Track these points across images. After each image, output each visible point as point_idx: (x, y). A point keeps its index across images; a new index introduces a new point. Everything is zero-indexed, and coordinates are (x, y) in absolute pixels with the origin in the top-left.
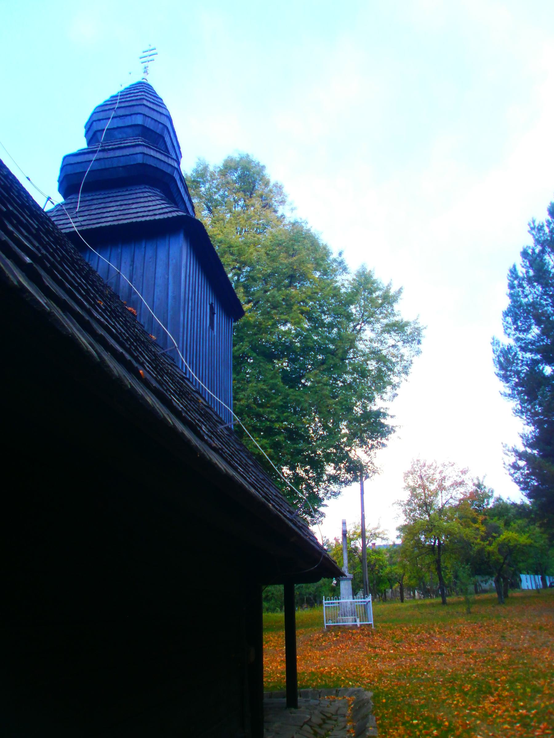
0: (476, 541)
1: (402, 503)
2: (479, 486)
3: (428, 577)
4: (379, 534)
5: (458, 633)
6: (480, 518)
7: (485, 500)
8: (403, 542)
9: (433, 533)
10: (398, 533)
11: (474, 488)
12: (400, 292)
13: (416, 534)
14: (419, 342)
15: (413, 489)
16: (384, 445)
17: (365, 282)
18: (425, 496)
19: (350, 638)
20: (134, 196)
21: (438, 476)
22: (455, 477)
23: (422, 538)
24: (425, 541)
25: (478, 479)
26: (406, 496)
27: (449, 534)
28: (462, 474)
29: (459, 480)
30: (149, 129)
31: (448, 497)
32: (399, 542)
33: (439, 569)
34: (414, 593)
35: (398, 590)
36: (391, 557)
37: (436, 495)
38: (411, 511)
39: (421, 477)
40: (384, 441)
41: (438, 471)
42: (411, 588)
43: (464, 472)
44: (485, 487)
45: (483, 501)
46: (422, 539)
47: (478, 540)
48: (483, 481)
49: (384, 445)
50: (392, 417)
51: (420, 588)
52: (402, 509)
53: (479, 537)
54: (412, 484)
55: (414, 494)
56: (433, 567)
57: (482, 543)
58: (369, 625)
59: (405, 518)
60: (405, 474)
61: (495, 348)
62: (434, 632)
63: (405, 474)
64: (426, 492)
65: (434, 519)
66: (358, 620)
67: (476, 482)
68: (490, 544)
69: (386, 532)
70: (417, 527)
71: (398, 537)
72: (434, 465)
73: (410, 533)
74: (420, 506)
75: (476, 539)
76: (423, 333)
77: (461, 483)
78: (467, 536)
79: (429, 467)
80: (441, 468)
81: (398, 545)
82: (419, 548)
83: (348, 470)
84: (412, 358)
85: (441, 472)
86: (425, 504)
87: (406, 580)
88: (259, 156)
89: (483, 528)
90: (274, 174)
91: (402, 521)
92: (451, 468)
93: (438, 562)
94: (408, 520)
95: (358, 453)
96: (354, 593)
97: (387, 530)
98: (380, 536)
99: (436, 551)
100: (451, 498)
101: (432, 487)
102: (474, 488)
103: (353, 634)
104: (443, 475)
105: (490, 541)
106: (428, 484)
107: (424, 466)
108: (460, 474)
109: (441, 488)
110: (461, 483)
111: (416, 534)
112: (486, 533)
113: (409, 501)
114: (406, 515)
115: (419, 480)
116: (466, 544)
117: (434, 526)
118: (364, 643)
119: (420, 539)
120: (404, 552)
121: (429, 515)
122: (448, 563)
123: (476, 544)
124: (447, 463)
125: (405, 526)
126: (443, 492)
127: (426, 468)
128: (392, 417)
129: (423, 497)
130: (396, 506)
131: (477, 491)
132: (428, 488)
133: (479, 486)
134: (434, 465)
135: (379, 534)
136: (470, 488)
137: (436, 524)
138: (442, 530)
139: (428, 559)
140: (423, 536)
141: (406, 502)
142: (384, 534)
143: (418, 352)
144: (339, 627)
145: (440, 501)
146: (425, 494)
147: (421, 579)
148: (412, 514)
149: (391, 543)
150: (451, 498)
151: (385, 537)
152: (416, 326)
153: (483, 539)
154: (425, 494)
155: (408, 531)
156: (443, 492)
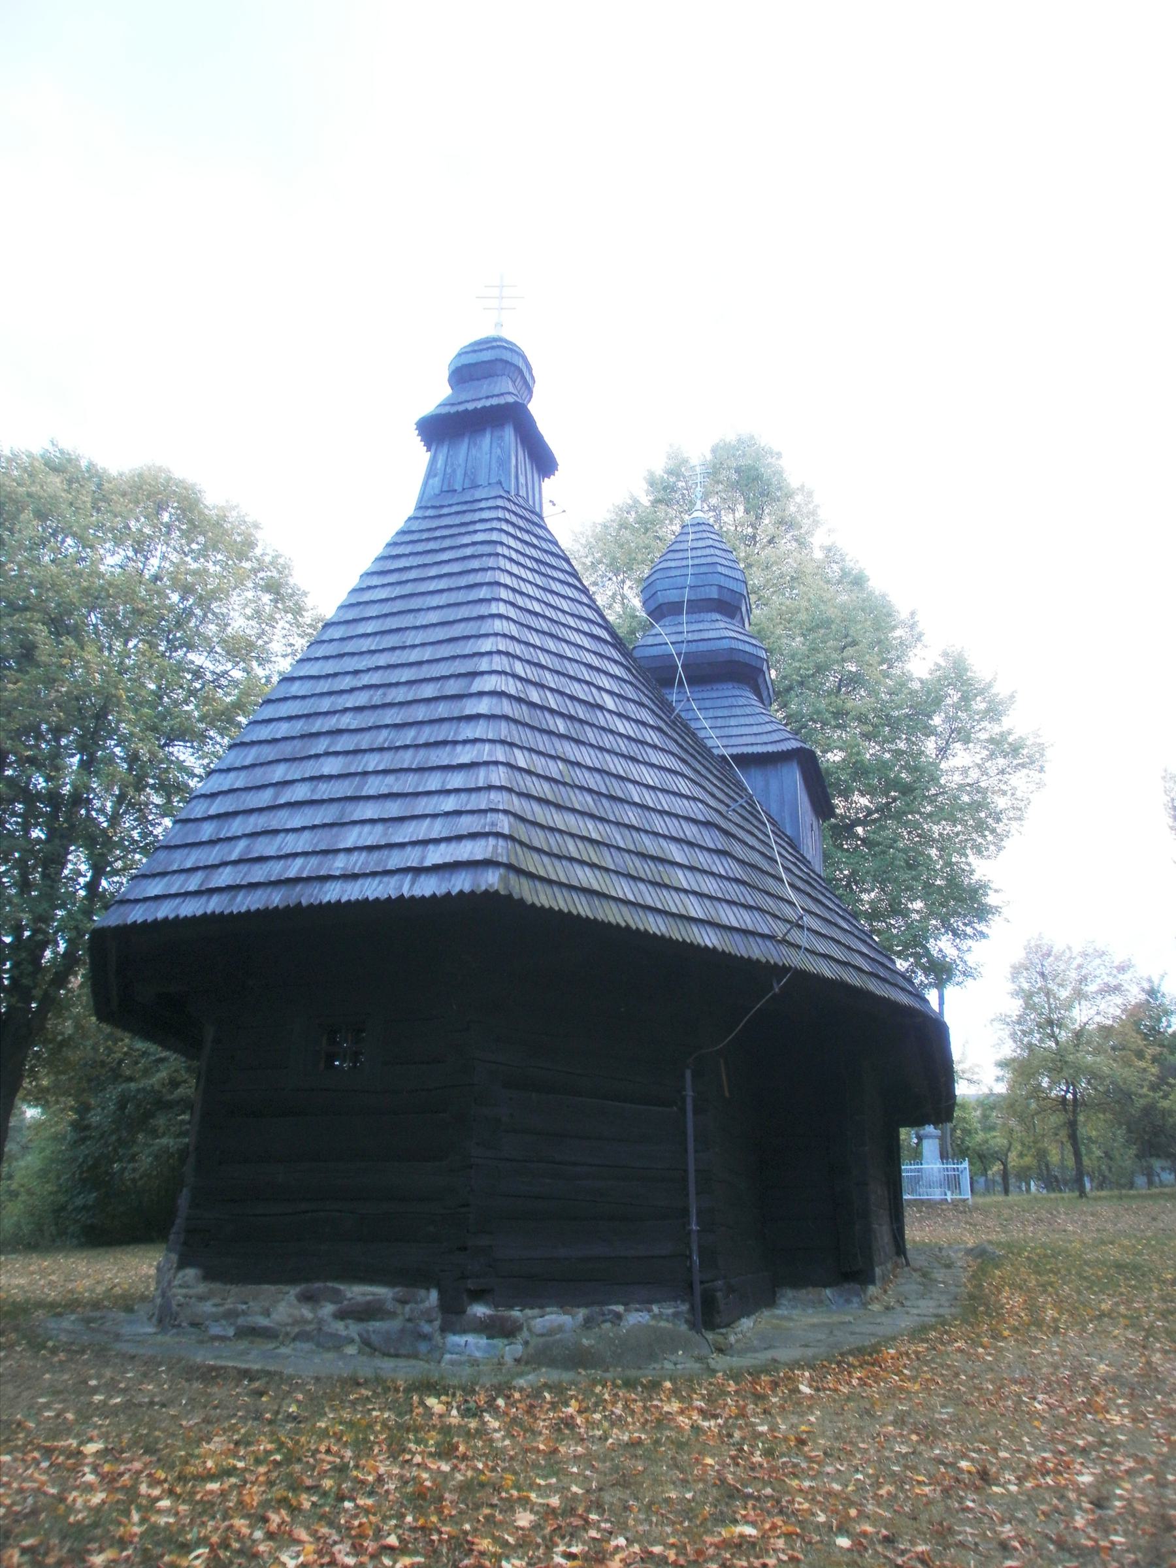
0: (1140, 1091)
1: (1008, 1020)
2: (1152, 993)
3: (1054, 1156)
4: (964, 1072)
5: (1092, 1215)
6: (1150, 1051)
7: (1164, 1019)
8: (1011, 1088)
9: (1065, 1074)
10: (999, 1072)
11: (1143, 996)
12: (1012, 697)
13: (1033, 1074)
14: (1041, 770)
15: (1028, 996)
16: (983, 935)
17: (956, 675)
18: (1050, 1008)
19: (939, 1215)
20: (726, 703)
21: (1073, 975)
22: (1104, 976)
23: (1045, 1083)
24: (1051, 1089)
25: (1150, 980)
26: (1015, 1007)
27: (1094, 1076)
28: (1119, 972)
29: (1113, 982)
30: (726, 603)
31: (1093, 1012)
32: (1001, 1088)
33: (1073, 1137)
34: (1028, 1185)
35: (998, 1179)
36: (985, 1117)
37: (1069, 1007)
38: (1024, 1033)
39: (1042, 975)
40: (981, 927)
41: (1074, 965)
42: (1024, 1175)
43: (1122, 969)
44: (1163, 996)
45: (1159, 1021)
46: (1045, 1085)
47: (1145, 1090)
48: (1159, 985)
49: (983, 935)
50: (996, 891)
51: (1040, 1177)
52: (1007, 1031)
53: (1146, 1083)
54: (1026, 986)
55: (1029, 1006)
56: (1063, 1133)
57: (1151, 1094)
58: (965, 1200)
59: (1014, 1046)
60: (1013, 967)
61: (1167, 785)
62: (1059, 1212)
63: (1013, 967)
64: (1052, 1001)
65: (1066, 1050)
66: (949, 1193)
67: (1146, 986)
68: (1165, 1097)
69: (976, 1070)
70: (1036, 1062)
71: (998, 1079)
72: (1068, 954)
73: (1022, 1074)
74: (1040, 1026)
75: (1142, 1087)
76: (1048, 753)
77: (1117, 989)
78: (1125, 1083)
79: (1057, 959)
80: (1079, 960)
81: (999, 1095)
82: (1038, 1098)
83: (927, 971)
84: (1031, 796)
85: (1080, 967)
86: (1050, 1023)
87: (1013, 1159)
88: (767, 439)
89: (1155, 1070)
90: (795, 469)
91: (1009, 1050)
92: (1098, 961)
93: (1072, 1125)
94: (1019, 1051)
95: (943, 946)
96: (944, 1156)
97: (978, 1066)
98: (966, 1076)
99: (1070, 1108)
100: (1098, 1013)
101: (1064, 994)
102: (1143, 996)
103: (943, 1210)
104: (1084, 972)
105: (1164, 1091)
106: (1055, 988)
107: (1049, 955)
108: (1115, 972)
109: (1079, 995)
110: (1117, 989)
111: (1033, 1074)
112: (1158, 1077)
113: (1020, 1016)
114: (1015, 1042)
115: (1039, 979)
116: (1124, 1096)
117: (1066, 1062)
118: (959, 1221)
119: (1040, 1085)
120: (1011, 1106)
121: (1057, 1043)
122: (1091, 1127)
123: (1141, 1096)
124: (1090, 951)
125: (1013, 1060)
126: (1083, 1002)
127: (1051, 958)
128: (996, 891)
129: (1046, 1011)
130: (997, 1025)
131: (1147, 1001)
132: (1054, 995)
133: (1152, 993)
134: (1068, 954)
135: (964, 1072)
136: (1136, 995)
137: (1070, 1058)
138: (1079, 1070)
139: (1055, 1119)
140: (1046, 1079)
141: (1015, 1018)
142: (973, 1074)
143: (1040, 785)
144: (922, 1202)
145: (1083, 1015)
146: (1050, 1005)
147: (1042, 1155)
148: (1026, 1039)
149: (987, 1091)
150: (1098, 1013)
151: (975, 1077)
152: (1038, 741)
153: (1154, 1088)
154: (1050, 1005)
155: (1021, 1071)
156: (1083, 1002)
